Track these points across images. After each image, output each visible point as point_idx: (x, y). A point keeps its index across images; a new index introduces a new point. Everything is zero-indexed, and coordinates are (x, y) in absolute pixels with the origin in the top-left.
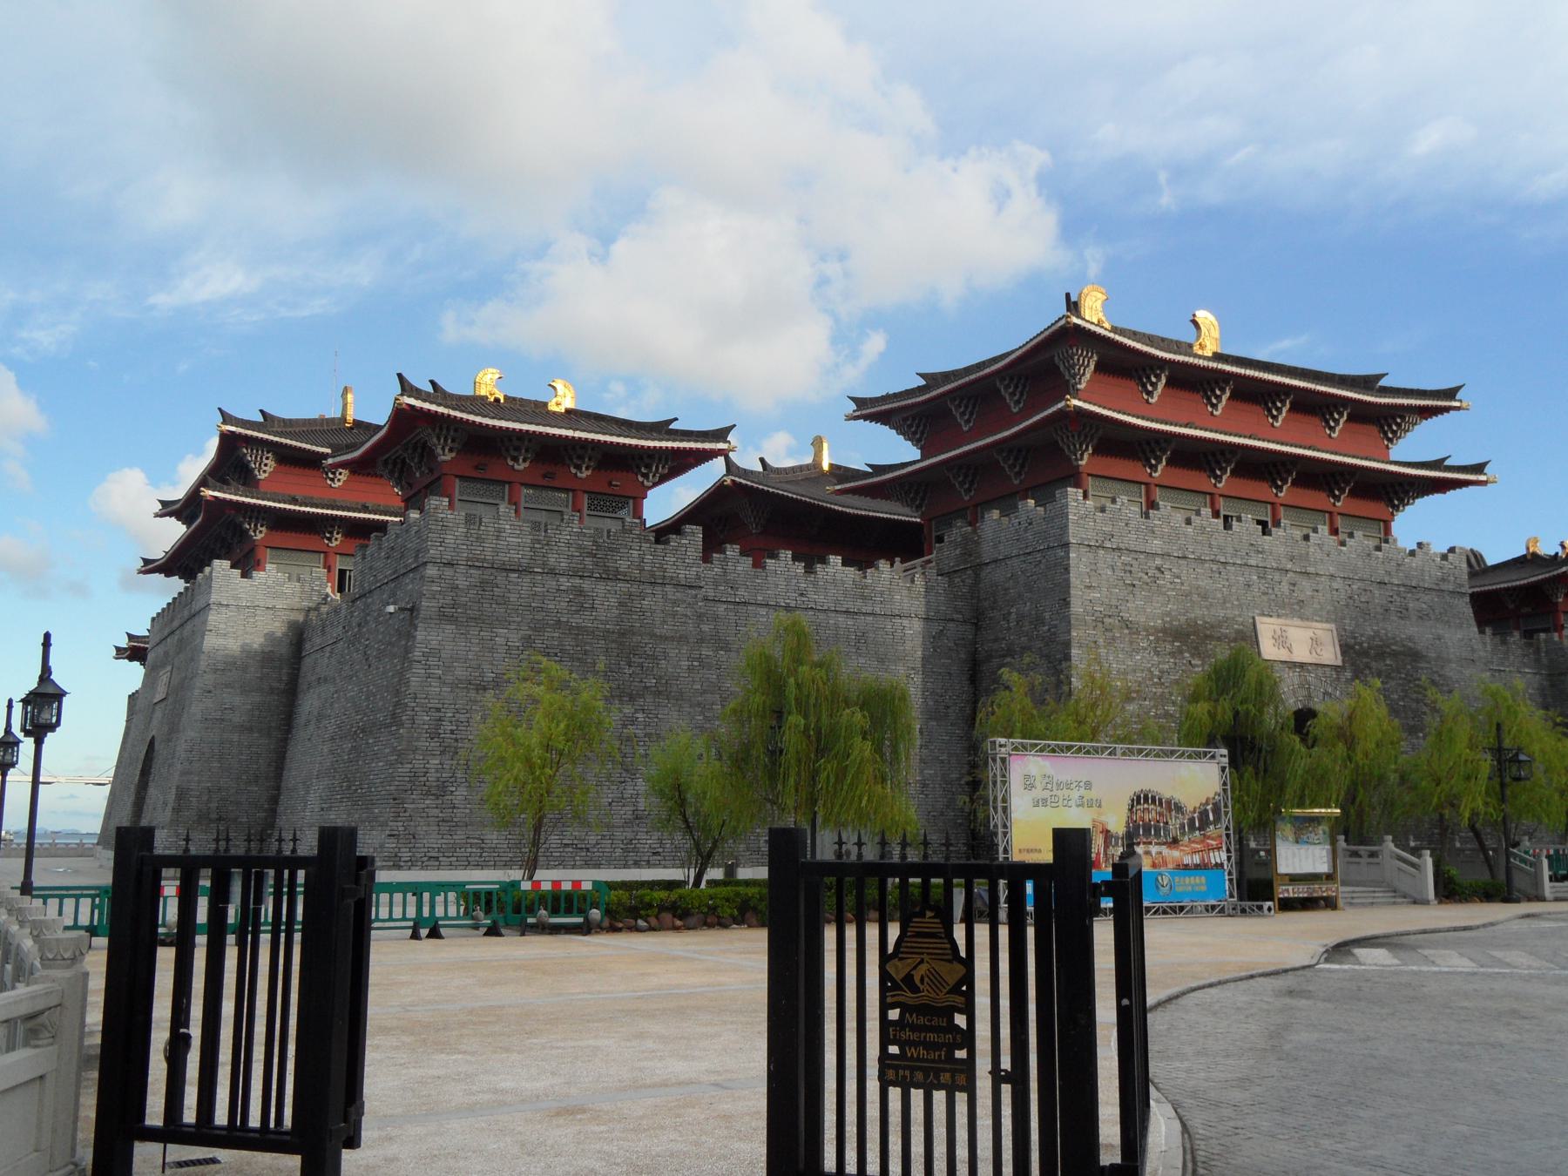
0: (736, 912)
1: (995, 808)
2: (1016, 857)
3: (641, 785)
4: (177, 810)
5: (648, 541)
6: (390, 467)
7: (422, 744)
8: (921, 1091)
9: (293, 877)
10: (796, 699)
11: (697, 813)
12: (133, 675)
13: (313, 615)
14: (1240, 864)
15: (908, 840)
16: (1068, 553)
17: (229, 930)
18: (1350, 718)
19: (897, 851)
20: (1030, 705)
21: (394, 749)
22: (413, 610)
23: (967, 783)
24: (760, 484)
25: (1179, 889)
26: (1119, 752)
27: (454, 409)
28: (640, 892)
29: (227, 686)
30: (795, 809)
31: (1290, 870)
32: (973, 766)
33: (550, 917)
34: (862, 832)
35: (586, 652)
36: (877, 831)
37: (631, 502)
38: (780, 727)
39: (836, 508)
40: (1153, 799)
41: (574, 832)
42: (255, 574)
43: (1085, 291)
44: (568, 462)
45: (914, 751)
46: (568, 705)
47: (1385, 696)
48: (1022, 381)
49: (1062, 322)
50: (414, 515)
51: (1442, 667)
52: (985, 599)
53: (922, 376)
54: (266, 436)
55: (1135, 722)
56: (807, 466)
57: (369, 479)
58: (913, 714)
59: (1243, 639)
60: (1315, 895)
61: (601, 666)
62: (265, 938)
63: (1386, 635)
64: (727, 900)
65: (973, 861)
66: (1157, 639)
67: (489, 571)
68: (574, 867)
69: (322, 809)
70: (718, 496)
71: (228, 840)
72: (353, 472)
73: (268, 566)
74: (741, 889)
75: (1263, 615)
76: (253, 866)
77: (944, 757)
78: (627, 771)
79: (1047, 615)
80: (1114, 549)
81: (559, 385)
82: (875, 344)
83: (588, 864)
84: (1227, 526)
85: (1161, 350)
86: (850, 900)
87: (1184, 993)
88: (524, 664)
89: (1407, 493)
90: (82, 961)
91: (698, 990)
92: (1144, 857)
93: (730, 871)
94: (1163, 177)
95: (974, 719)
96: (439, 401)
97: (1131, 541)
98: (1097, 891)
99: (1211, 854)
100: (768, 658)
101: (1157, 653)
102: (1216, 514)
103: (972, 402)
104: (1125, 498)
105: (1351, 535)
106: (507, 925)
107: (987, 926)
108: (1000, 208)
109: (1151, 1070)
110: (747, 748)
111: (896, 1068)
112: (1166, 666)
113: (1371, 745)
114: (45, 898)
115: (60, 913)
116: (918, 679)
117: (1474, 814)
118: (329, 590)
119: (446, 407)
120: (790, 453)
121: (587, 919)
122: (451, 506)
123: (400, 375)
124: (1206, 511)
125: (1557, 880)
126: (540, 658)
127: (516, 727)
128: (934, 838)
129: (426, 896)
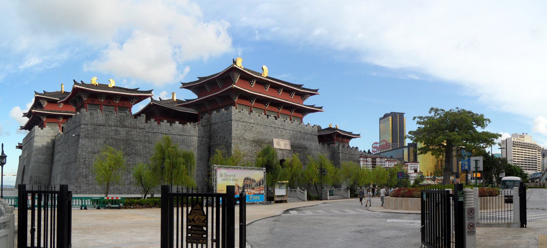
0: (153, 204)
1: (213, 181)
2: (218, 192)
3: (132, 176)
4: (30, 181)
5: (133, 118)
6: (72, 102)
7: (82, 166)
8: (196, 244)
9: (55, 195)
10: (168, 155)
11: (144, 182)
12: (20, 152)
13: (57, 137)
14: (267, 193)
15: (193, 188)
16: (232, 122)
17: (42, 206)
18: (292, 161)
19: (191, 191)
20: (222, 157)
21: (75, 167)
22: (79, 135)
23: (207, 175)
24: (159, 104)
25: (254, 199)
27: (87, 87)
28: (132, 200)
29: (39, 154)
30: (167, 181)
31: (278, 195)
32: (209, 171)
33: (111, 205)
34: (183, 186)
35: (118, 145)
36: (186, 186)
37: (128, 108)
38: (164, 162)
39: (177, 110)
40: (249, 179)
41: (116, 186)
42: (44, 128)
43: (238, 59)
44: (113, 99)
45: (195, 167)
46: (114, 157)
47: (299, 157)
48: (222, 80)
49: (232, 66)
50: (78, 113)
51: (311, 151)
52: (213, 132)
53: (198, 78)
54: (45, 97)
55: (246, 162)
56: (171, 99)
57: (68, 105)
58: (195, 159)
59: (270, 143)
60: (283, 200)
61: (122, 148)
62: (49, 209)
64: (152, 202)
65: (208, 193)
66: (251, 143)
67: (96, 126)
68: (116, 194)
69: (60, 181)
70: (149, 107)
71: (41, 187)
72: (64, 104)
73: (47, 127)
74: (155, 199)
75: (275, 138)
76: (46, 193)
77: (202, 169)
78: (128, 172)
79: (226, 136)
80: (242, 121)
81: (111, 80)
82: (187, 69)
83: (119, 193)
84: (268, 117)
85: (255, 74)
86: (180, 202)
87: (254, 222)
88: (104, 147)
89: (306, 112)
90: (13, 212)
91: (145, 222)
92: (246, 192)
93: (152, 195)
94: (257, 32)
95: (209, 160)
96: (83, 86)
98: (236, 199)
100: (161, 146)
101: (251, 146)
102: (265, 114)
103: (210, 84)
104: (245, 110)
105: (294, 121)
106: (102, 207)
107: (211, 208)
108: (218, 36)
109: (246, 238)
110: (156, 167)
111: (190, 239)
112: (253, 149)
113: (295, 168)
114: (5, 199)
115: (8, 202)
116: (196, 151)
117: (315, 182)
118: (60, 131)
119: (85, 87)
120: (167, 96)
121: (119, 206)
122: (86, 111)
123: (74, 80)
124: (263, 114)
125: (330, 196)
126: (108, 146)
127: (103, 162)
128: (199, 188)
129: (83, 200)
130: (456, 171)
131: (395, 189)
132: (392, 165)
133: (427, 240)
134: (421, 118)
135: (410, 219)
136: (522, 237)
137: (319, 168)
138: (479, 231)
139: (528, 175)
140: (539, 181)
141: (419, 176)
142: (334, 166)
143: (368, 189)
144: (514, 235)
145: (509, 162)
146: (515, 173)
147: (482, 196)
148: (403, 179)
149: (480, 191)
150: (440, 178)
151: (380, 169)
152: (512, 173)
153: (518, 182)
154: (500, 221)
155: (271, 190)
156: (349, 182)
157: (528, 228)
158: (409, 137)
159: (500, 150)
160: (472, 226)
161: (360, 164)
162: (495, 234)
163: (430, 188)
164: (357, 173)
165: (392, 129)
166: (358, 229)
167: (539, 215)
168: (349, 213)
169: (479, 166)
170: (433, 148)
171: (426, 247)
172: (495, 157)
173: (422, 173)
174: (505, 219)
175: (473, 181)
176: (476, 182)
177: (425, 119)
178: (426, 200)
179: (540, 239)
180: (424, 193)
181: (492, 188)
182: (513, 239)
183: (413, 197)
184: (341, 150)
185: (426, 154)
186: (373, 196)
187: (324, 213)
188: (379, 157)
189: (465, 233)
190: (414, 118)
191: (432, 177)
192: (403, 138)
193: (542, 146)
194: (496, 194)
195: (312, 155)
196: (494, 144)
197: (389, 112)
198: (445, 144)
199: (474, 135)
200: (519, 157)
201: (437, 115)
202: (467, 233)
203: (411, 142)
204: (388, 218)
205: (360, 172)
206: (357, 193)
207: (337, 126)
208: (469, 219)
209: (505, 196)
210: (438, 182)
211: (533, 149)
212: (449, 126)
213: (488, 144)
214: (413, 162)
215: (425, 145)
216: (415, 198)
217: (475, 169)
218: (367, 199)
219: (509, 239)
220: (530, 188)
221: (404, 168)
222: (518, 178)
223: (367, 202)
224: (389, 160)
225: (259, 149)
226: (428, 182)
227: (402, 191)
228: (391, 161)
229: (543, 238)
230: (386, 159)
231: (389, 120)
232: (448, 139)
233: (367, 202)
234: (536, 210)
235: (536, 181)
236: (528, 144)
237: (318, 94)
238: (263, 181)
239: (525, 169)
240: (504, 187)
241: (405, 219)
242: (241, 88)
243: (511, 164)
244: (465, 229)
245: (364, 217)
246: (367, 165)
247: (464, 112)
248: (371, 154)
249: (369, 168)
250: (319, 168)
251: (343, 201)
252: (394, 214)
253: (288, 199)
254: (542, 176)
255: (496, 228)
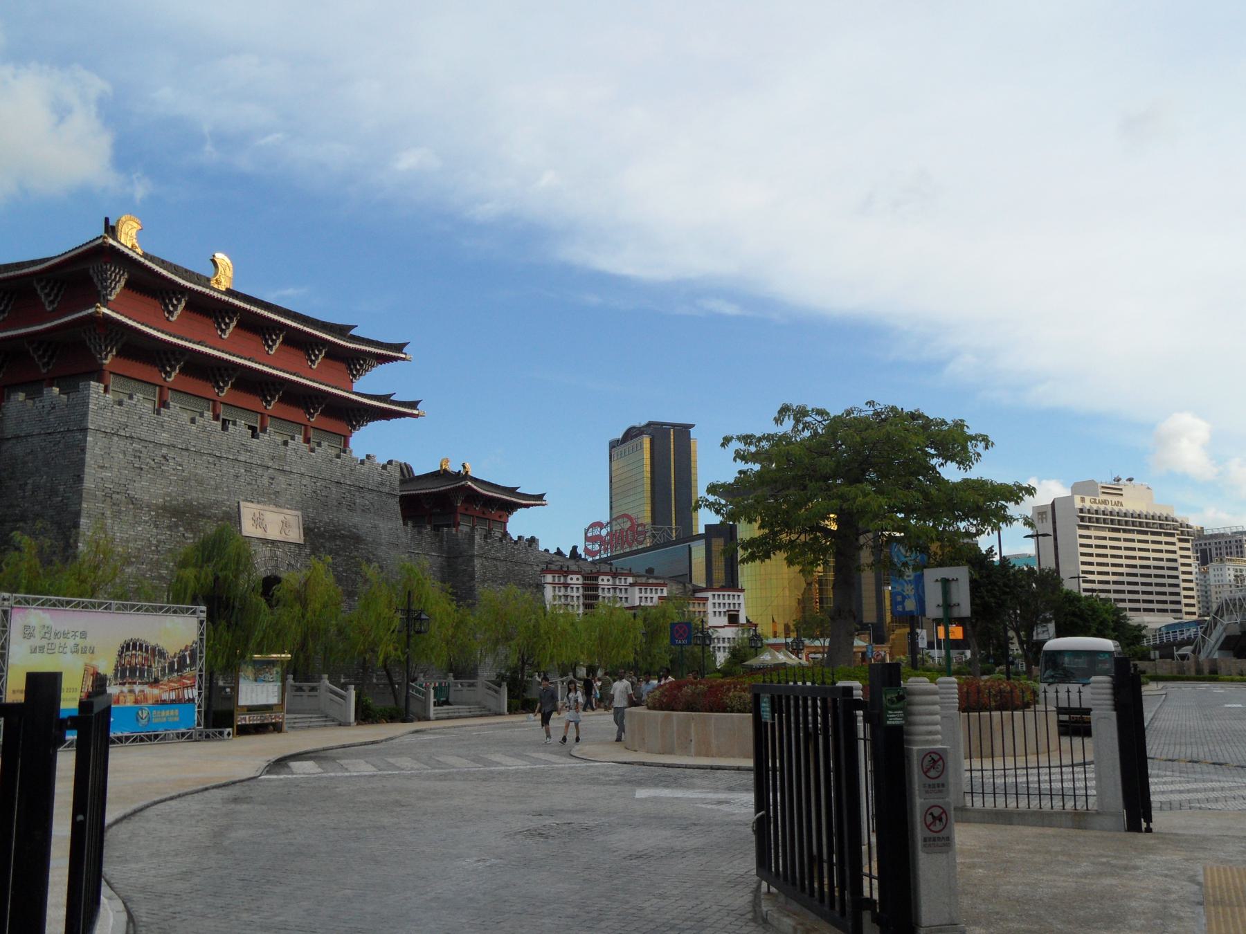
14: (209, 699)
18: (305, 584)
26: (114, 607)
31: (248, 703)
40: (141, 645)
43: (123, 219)
49: (100, 241)
60: (266, 722)
63: (338, 522)
66: (158, 515)
75: (246, 500)
79: (61, 488)
84: (225, 428)
87: (147, 807)
97: (142, 431)
98: (64, 725)
99: (186, 691)
101: (156, 526)
102: (216, 417)
104: (141, 396)
105: (319, 445)
113: (318, 606)
117: (386, 659)
124: (208, 414)
125: (439, 705)
130: (874, 620)
131: (663, 682)
132: (652, 598)
133: (778, 863)
134: (747, 439)
135: (716, 790)
136: (1136, 868)
137: (400, 608)
138: (964, 836)
139: (1144, 632)
140: (1194, 652)
141: (745, 636)
142: (453, 600)
143: (570, 682)
144: (1104, 860)
145: (1069, 585)
146: (1094, 626)
147: (974, 710)
148: (688, 648)
149: (965, 690)
150: (817, 643)
151: (611, 614)
152: (1081, 623)
153: (1107, 656)
154: (1046, 804)
155: (224, 688)
156: (506, 657)
157: (1158, 833)
158: (710, 505)
159: (1032, 541)
160: (940, 820)
161: (543, 594)
162: (1029, 851)
163: (783, 677)
164: (534, 626)
165: (652, 478)
166: (536, 823)
167: (1201, 785)
168: (503, 768)
169: (955, 600)
170: (791, 542)
171: (773, 889)
172: (1014, 566)
173: (756, 626)
174: (1063, 795)
175: (936, 653)
176: (948, 658)
177: (764, 444)
178: (769, 721)
179: (1213, 880)
180: (761, 695)
181: (1009, 678)
182: (1101, 874)
183: (724, 711)
184: (481, 547)
185: (766, 560)
186: (588, 706)
187: (416, 767)
188: (608, 570)
189: (914, 842)
190: (727, 441)
191: (789, 640)
192: (688, 507)
193: (1195, 522)
194: (1026, 700)
195: (378, 562)
196: (1009, 520)
197: (640, 421)
198: (834, 527)
199: (933, 491)
200: (1107, 565)
201: (803, 430)
202: (920, 844)
203: (716, 519)
204: (640, 783)
205: (541, 622)
206: (533, 694)
207: (467, 465)
208: (927, 792)
209: (1060, 711)
210: (812, 656)
211: (1159, 534)
212: (845, 466)
213: (985, 520)
214: (722, 588)
215: (762, 532)
216: (732, 712)
217: (941, 609)
218: (566, 715)
219: (1085, 875)
220: (1157, 679)
221: (694, 608)
222: (1107, 644)
223: (567, 726)
224: (644, 580)
225: (186, 538)
226: (777, 658)
227: (688, 690)
228: (653, 585)
229: (1226, 879)
230: (630, 580)
231: (642, 448)
232: (844, 510)
233: (567, 726)
234: (1190, 765)
235: (1180, 652)
236: (1139, 516)
237: (404, 359)
238: (193, 656)
239: (1131, 610)
240: (1052, 677)
241: (699, 787)
242: (130, 319)
243: (1076, 590)
244: (913, 829)
245: (557, 780)
246: (566, 600)
247: (894, 416)
248: (581, 562)
249: (576, 608)
250: (400, 608)
251: (482, 725)
252: (659, 770)
253: (286, 718)
254: (1205, 633)
255: (1030, 828)
